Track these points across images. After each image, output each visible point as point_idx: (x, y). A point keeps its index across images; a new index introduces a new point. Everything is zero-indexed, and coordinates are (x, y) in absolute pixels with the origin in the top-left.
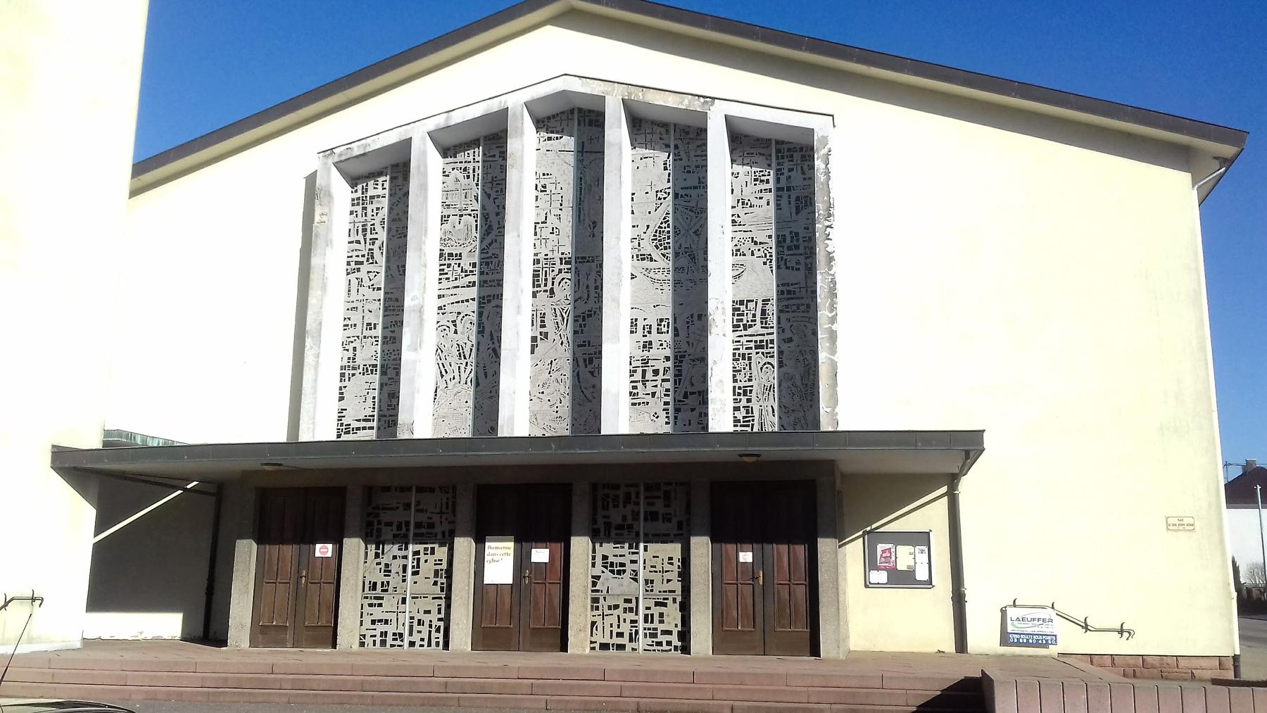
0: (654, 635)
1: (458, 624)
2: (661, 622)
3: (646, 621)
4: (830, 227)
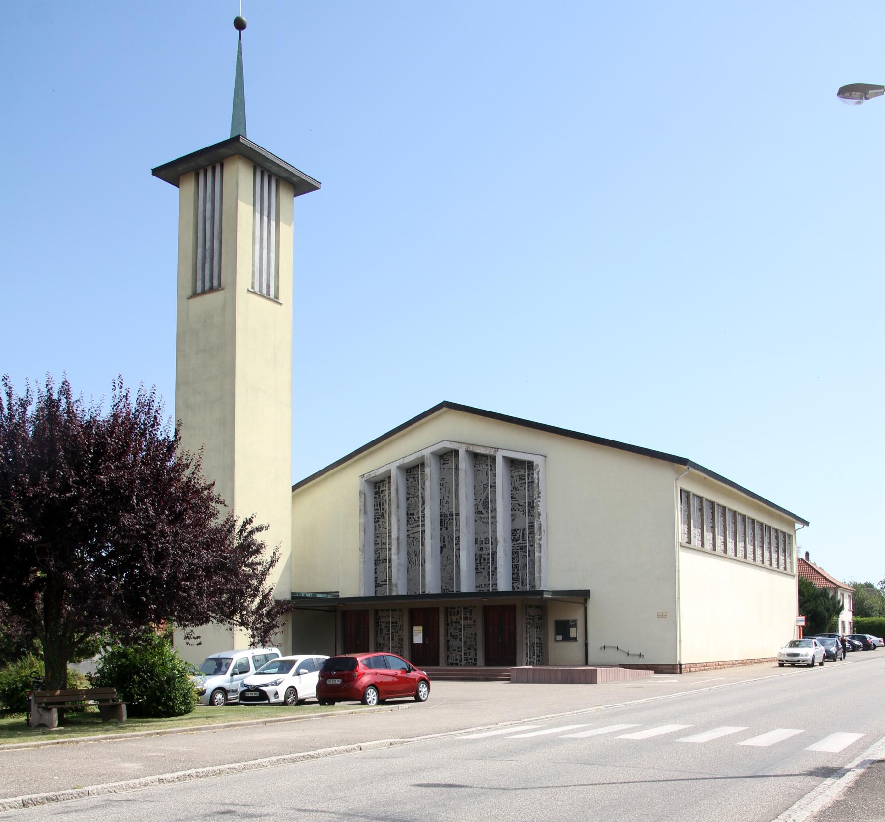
0: (467, 660)
1: (777, 780)
2: (469, 655)
3: (464, 655)
4: (539, 501)
